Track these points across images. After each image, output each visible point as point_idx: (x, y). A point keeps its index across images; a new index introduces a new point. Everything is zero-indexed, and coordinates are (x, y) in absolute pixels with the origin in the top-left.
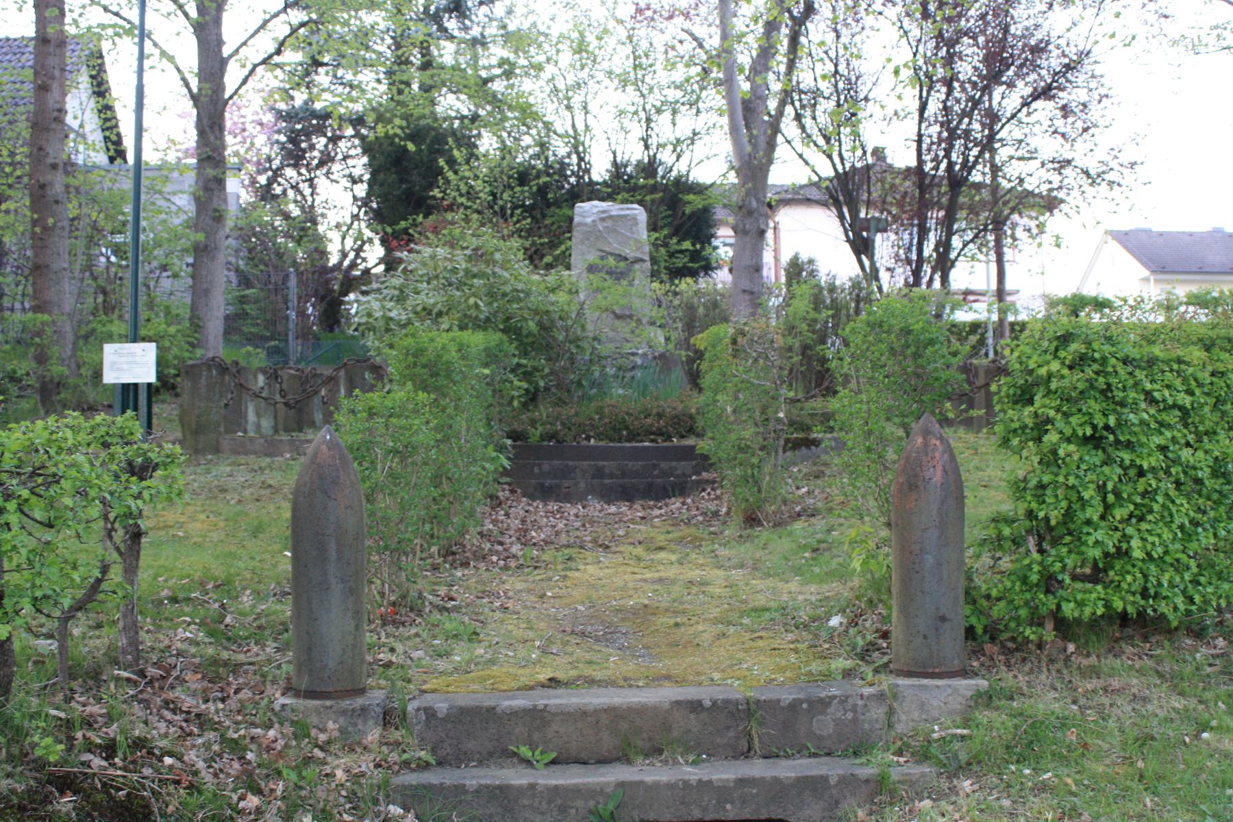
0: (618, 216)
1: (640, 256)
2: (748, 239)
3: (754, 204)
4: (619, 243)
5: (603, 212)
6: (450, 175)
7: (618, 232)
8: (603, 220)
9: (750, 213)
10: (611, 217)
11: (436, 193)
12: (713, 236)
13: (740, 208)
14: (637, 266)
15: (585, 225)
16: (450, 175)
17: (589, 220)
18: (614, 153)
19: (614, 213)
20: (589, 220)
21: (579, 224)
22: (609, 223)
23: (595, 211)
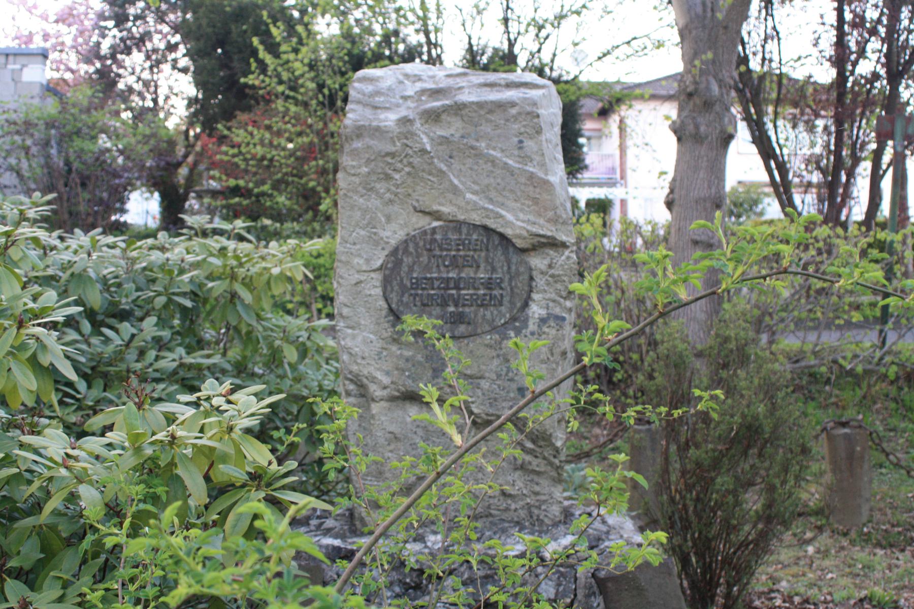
0: (480, 105)
1: (547, 230)
2: (703, 150)
3: (715, 88)
4: (484, 191)
5: (436, 93)
6: (268, 59)
7: (479, 155)
8: (433, 117)
9: (708, 105)
10: (458, 109)
11: (251, 80)
12: (580, 130)
13: (690, 95)
14: (537, 262)
15: (378, 132)
16: (268, 59)
17: (389, 119)
18: (470, 38)
19: (466, 97)
20: (389, 119)
21: (360, 132)
22: (452, 128)
23: (411, 89)
